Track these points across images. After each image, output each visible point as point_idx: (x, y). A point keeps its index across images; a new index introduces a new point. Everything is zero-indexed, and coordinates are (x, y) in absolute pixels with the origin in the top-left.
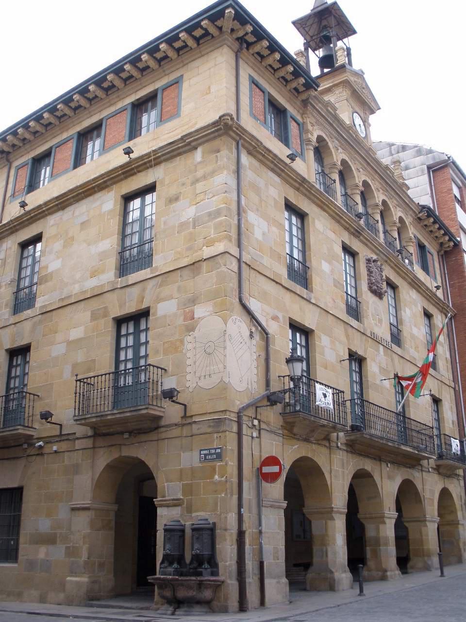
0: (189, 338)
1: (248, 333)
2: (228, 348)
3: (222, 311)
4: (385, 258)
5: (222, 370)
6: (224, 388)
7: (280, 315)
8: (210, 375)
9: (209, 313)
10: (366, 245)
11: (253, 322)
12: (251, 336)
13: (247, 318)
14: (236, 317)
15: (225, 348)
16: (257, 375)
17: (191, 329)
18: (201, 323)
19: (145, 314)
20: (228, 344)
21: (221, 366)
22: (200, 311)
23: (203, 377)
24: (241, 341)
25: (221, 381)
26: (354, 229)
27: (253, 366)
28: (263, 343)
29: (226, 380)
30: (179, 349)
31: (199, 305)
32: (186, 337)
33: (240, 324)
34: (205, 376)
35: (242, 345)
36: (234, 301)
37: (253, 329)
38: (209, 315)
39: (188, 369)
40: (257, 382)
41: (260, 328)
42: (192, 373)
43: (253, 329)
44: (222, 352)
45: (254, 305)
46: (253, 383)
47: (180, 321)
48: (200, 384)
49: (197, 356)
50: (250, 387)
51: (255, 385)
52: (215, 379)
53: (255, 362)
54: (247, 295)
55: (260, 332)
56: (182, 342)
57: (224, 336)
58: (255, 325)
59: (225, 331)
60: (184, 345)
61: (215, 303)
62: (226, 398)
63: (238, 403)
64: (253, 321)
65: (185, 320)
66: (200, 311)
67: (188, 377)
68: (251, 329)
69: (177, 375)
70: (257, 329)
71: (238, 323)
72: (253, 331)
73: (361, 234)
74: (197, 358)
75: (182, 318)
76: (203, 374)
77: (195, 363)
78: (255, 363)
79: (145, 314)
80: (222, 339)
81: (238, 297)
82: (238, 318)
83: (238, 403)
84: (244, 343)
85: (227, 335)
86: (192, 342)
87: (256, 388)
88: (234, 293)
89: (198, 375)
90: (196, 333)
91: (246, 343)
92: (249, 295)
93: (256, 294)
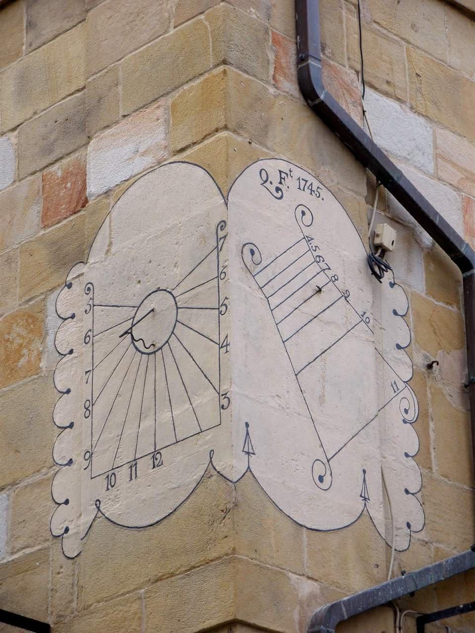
0: (66, 301)
1: (358, 252)
2: (237, 308)
3: (214, 144)
5: (209, 416)
6: (227, 503)
8: (155, 455)
9: (149, 160)
11: (386, 206)
12: (377, 261)
13: (354, 183)
14: (284, 166)
15: (222, 308)
16: (422, 457)
17: (70, 255)
18: (114, 214)
19: (71, 459)
20: (237, 280)
21: (206, 399)
22: (107, 162)
23: (123, 474)
24: (321, 280)
25: (207, 476)
27: (394, 415)
28: (454, 309)
29: (233, 464)
30: (23, 361)
31: (107, 132)
32: (53, 297)
33: (305, 197)
34: (133, 465)
35: (317, 305)
36: (272, 90)
37: (388, 235)
38: (151, 170)
39: (64, 447)
40: (423, 495)
41: (427, 238)
42: (79, 461)
43: (388, 235)
44: (210, 328)
45: (389, 126)
46: (397, 496)
47: (29, 226)
48: (109, 509)
49: (100, 375)
50: (378, 515)
51: (409, 510)
52: (181, 471)
53: (407, 393)
54: (350, 76)
55: (431, 256)
56: (34, 321)
57: (218, 249)
58: (395, 220)
59: (222, 225)
60: (43, 336)
61: (174, 105)
62: (230, 558)
63: (307, 588)
64: (383, 199)
65: (46, 219)
66: (107, 162)
67: (62, 487)
68: (374, 235)
69: (14, 484)
70: (411, 239)
71: (293, 194)
72: (387, 243)
74: (98, 382)
75: (34, 213)
76: (126, 456)
77: (88, 409)
78: (407, 400)
79: (71, 459)
80: (209, 269)
81: (293, 71)
82: (297, 173)
83: (307, 588)
84: (331, 294)
85: (232, 245)
86: (79, 312)
87: (417, 525)
88: (271, 56)
89: (101, 464)
90: (95, 268)
91: (346, 295)
92: (361, 73)
93: (401, 79)
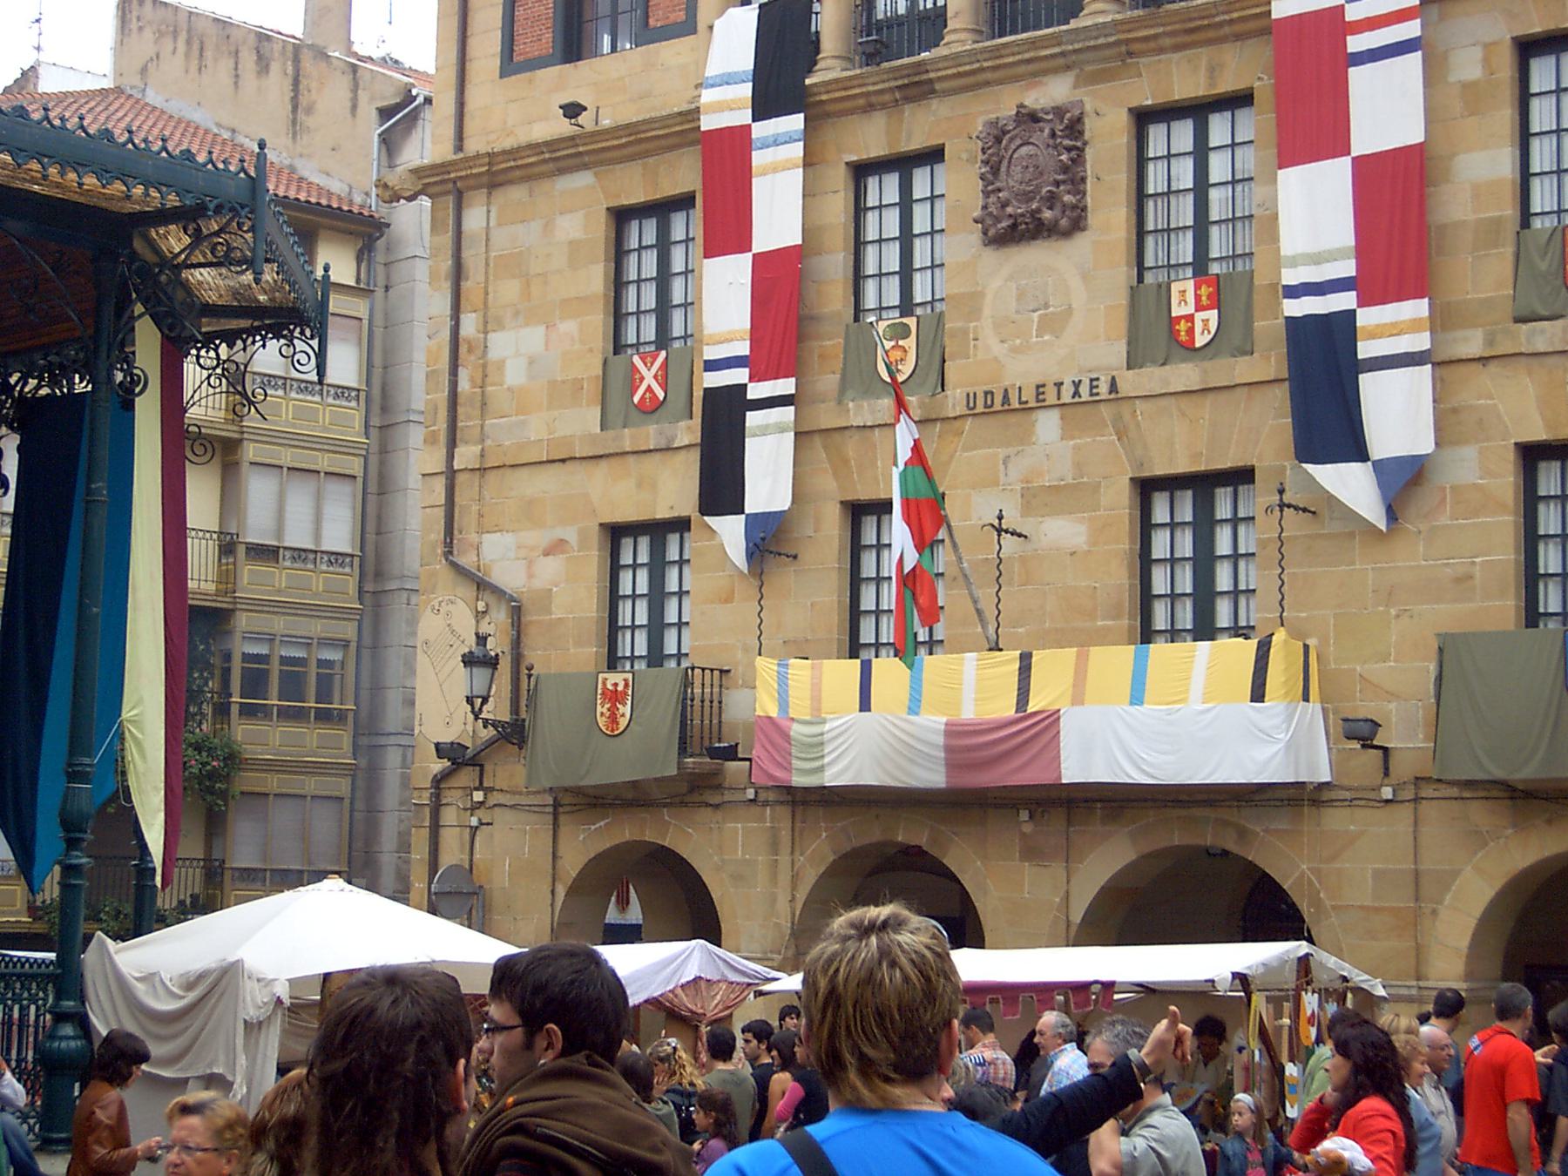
4: (1115, 51)
7: (570, 534)
10: (987, 83)
26: (891, 90)
73: (931, 81)
